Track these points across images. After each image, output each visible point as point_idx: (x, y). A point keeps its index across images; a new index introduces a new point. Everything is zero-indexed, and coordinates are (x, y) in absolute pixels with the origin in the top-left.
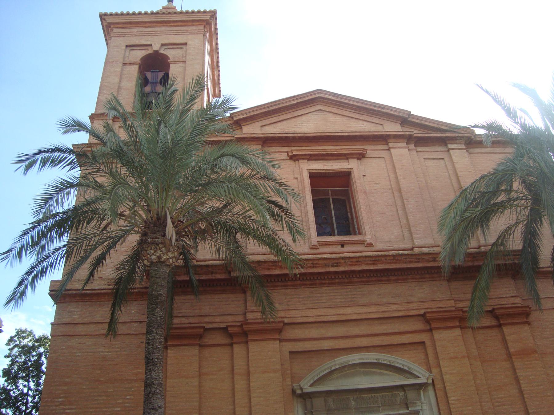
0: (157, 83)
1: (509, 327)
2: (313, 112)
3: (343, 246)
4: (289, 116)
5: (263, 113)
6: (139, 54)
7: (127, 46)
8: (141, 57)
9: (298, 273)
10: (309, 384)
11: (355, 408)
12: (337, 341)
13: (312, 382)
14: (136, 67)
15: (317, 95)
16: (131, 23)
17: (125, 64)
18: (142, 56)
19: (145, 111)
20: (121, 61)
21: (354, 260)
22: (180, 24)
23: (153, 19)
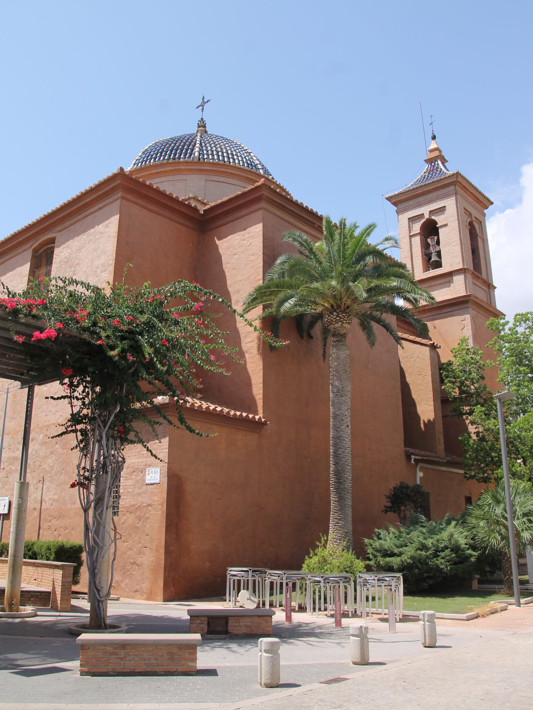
7: (409, 219)
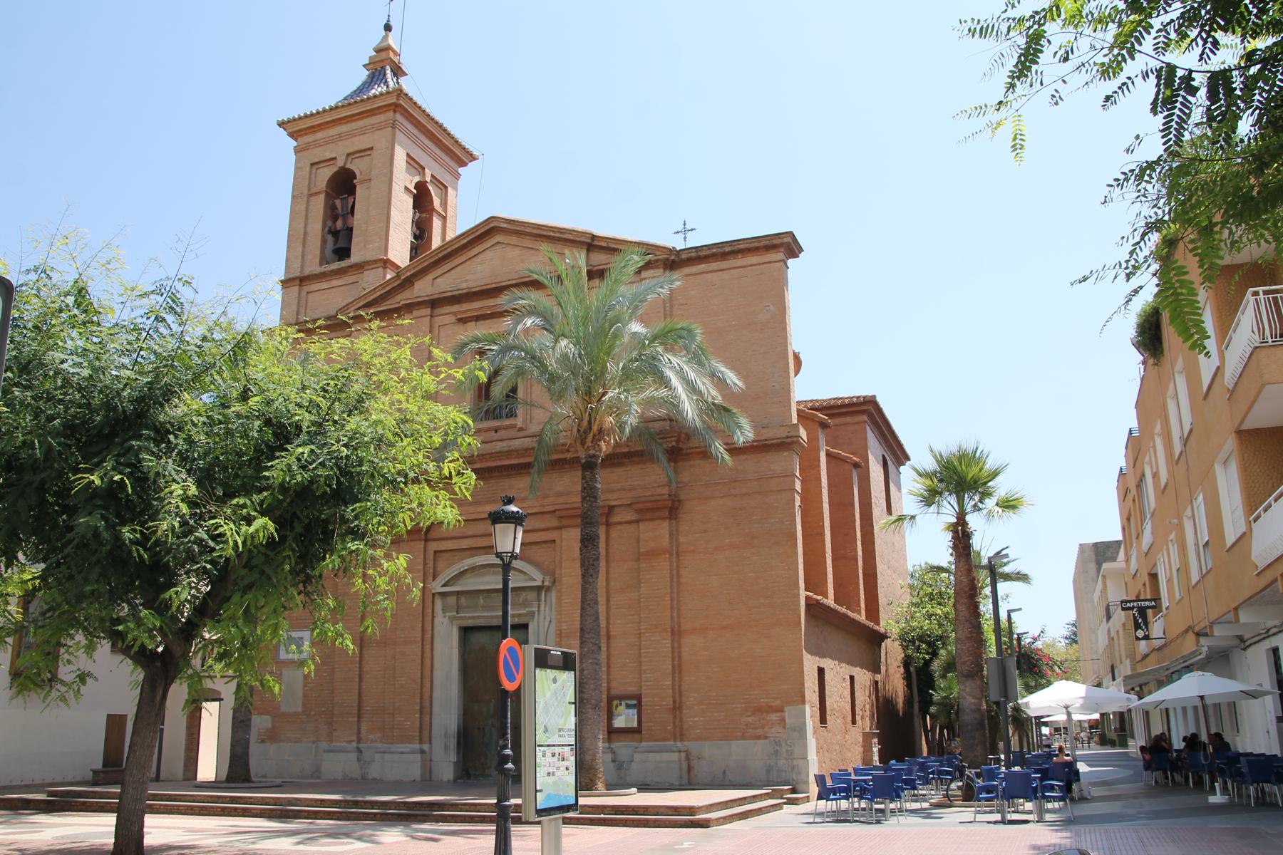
0: (348, 214)
1: (647, 523)
2: (491, 247)
3: (496, 431)
4: (463, 258)
5: (433, 263)
6: (326, 173)
8: (327, 179)
9: (142, 643)
10: (441, 584)
11: (482, 607)
12: (475, 540)
13: (443, 582)
14: (322, 196)
15: (492, 225)
16: (312, 127)
17: (310, 195)
18: (329, 177)
19: (109, 584)
20: (306, 192)
21: (487, 457)
22: (365, 115)
23: (334, 116)
